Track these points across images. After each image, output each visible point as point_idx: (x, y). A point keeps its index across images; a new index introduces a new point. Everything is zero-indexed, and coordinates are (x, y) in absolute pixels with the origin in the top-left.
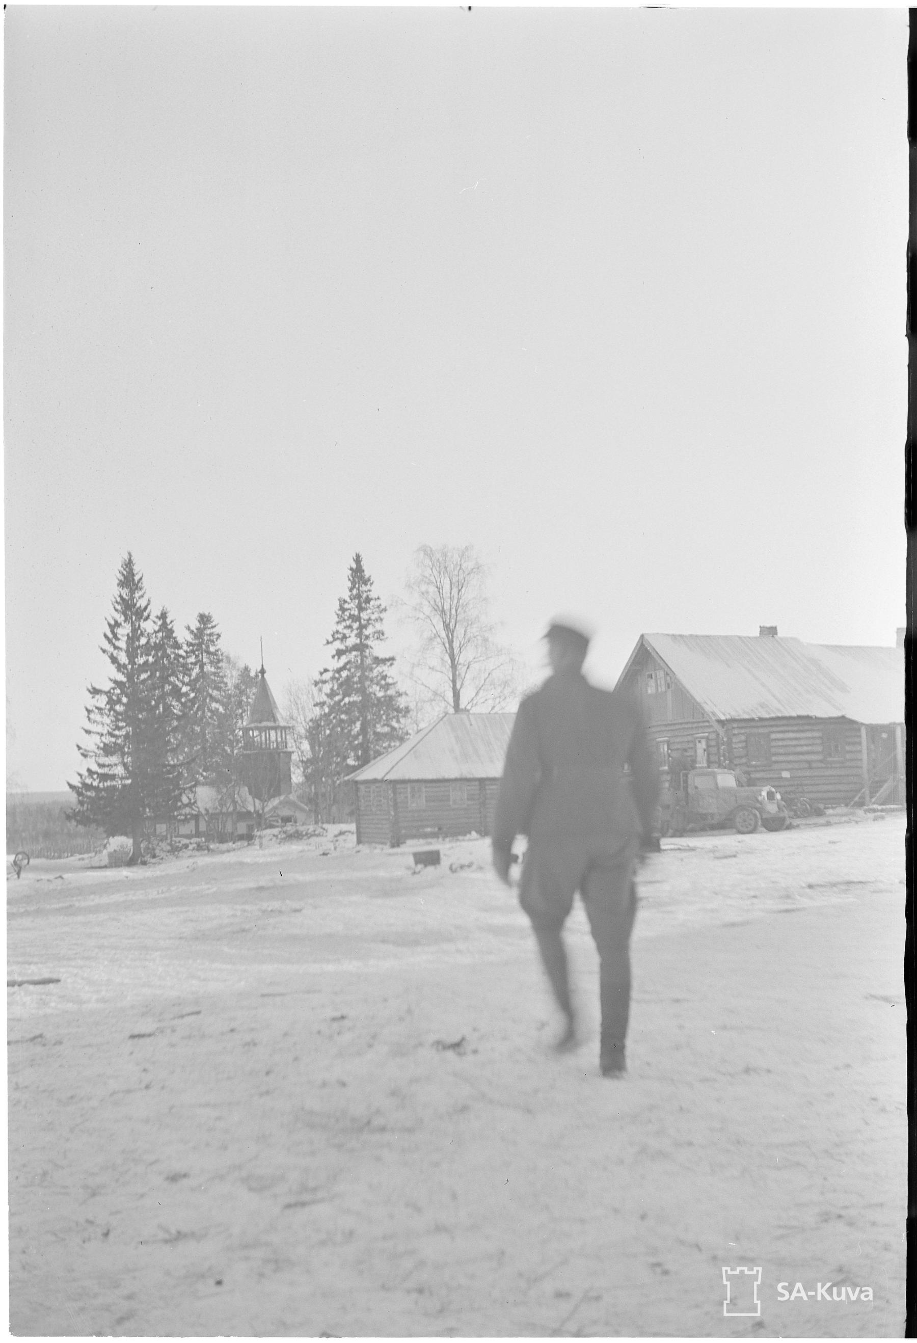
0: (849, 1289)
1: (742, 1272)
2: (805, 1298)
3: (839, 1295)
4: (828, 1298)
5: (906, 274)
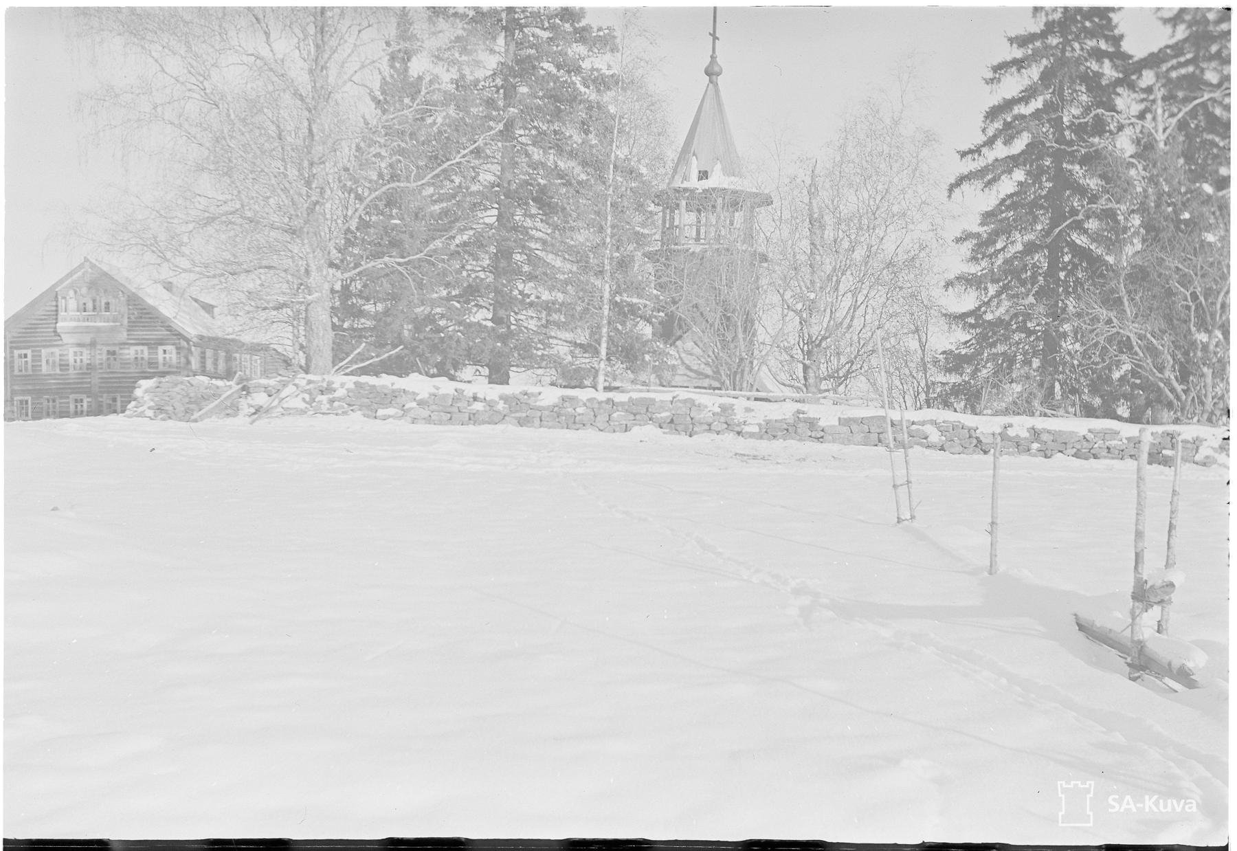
0: (1175, 802)
1: (1067, 783)
2: (1134, 810)
3: (1165, 807)
4: (1155, 809)
5: (980, 842)
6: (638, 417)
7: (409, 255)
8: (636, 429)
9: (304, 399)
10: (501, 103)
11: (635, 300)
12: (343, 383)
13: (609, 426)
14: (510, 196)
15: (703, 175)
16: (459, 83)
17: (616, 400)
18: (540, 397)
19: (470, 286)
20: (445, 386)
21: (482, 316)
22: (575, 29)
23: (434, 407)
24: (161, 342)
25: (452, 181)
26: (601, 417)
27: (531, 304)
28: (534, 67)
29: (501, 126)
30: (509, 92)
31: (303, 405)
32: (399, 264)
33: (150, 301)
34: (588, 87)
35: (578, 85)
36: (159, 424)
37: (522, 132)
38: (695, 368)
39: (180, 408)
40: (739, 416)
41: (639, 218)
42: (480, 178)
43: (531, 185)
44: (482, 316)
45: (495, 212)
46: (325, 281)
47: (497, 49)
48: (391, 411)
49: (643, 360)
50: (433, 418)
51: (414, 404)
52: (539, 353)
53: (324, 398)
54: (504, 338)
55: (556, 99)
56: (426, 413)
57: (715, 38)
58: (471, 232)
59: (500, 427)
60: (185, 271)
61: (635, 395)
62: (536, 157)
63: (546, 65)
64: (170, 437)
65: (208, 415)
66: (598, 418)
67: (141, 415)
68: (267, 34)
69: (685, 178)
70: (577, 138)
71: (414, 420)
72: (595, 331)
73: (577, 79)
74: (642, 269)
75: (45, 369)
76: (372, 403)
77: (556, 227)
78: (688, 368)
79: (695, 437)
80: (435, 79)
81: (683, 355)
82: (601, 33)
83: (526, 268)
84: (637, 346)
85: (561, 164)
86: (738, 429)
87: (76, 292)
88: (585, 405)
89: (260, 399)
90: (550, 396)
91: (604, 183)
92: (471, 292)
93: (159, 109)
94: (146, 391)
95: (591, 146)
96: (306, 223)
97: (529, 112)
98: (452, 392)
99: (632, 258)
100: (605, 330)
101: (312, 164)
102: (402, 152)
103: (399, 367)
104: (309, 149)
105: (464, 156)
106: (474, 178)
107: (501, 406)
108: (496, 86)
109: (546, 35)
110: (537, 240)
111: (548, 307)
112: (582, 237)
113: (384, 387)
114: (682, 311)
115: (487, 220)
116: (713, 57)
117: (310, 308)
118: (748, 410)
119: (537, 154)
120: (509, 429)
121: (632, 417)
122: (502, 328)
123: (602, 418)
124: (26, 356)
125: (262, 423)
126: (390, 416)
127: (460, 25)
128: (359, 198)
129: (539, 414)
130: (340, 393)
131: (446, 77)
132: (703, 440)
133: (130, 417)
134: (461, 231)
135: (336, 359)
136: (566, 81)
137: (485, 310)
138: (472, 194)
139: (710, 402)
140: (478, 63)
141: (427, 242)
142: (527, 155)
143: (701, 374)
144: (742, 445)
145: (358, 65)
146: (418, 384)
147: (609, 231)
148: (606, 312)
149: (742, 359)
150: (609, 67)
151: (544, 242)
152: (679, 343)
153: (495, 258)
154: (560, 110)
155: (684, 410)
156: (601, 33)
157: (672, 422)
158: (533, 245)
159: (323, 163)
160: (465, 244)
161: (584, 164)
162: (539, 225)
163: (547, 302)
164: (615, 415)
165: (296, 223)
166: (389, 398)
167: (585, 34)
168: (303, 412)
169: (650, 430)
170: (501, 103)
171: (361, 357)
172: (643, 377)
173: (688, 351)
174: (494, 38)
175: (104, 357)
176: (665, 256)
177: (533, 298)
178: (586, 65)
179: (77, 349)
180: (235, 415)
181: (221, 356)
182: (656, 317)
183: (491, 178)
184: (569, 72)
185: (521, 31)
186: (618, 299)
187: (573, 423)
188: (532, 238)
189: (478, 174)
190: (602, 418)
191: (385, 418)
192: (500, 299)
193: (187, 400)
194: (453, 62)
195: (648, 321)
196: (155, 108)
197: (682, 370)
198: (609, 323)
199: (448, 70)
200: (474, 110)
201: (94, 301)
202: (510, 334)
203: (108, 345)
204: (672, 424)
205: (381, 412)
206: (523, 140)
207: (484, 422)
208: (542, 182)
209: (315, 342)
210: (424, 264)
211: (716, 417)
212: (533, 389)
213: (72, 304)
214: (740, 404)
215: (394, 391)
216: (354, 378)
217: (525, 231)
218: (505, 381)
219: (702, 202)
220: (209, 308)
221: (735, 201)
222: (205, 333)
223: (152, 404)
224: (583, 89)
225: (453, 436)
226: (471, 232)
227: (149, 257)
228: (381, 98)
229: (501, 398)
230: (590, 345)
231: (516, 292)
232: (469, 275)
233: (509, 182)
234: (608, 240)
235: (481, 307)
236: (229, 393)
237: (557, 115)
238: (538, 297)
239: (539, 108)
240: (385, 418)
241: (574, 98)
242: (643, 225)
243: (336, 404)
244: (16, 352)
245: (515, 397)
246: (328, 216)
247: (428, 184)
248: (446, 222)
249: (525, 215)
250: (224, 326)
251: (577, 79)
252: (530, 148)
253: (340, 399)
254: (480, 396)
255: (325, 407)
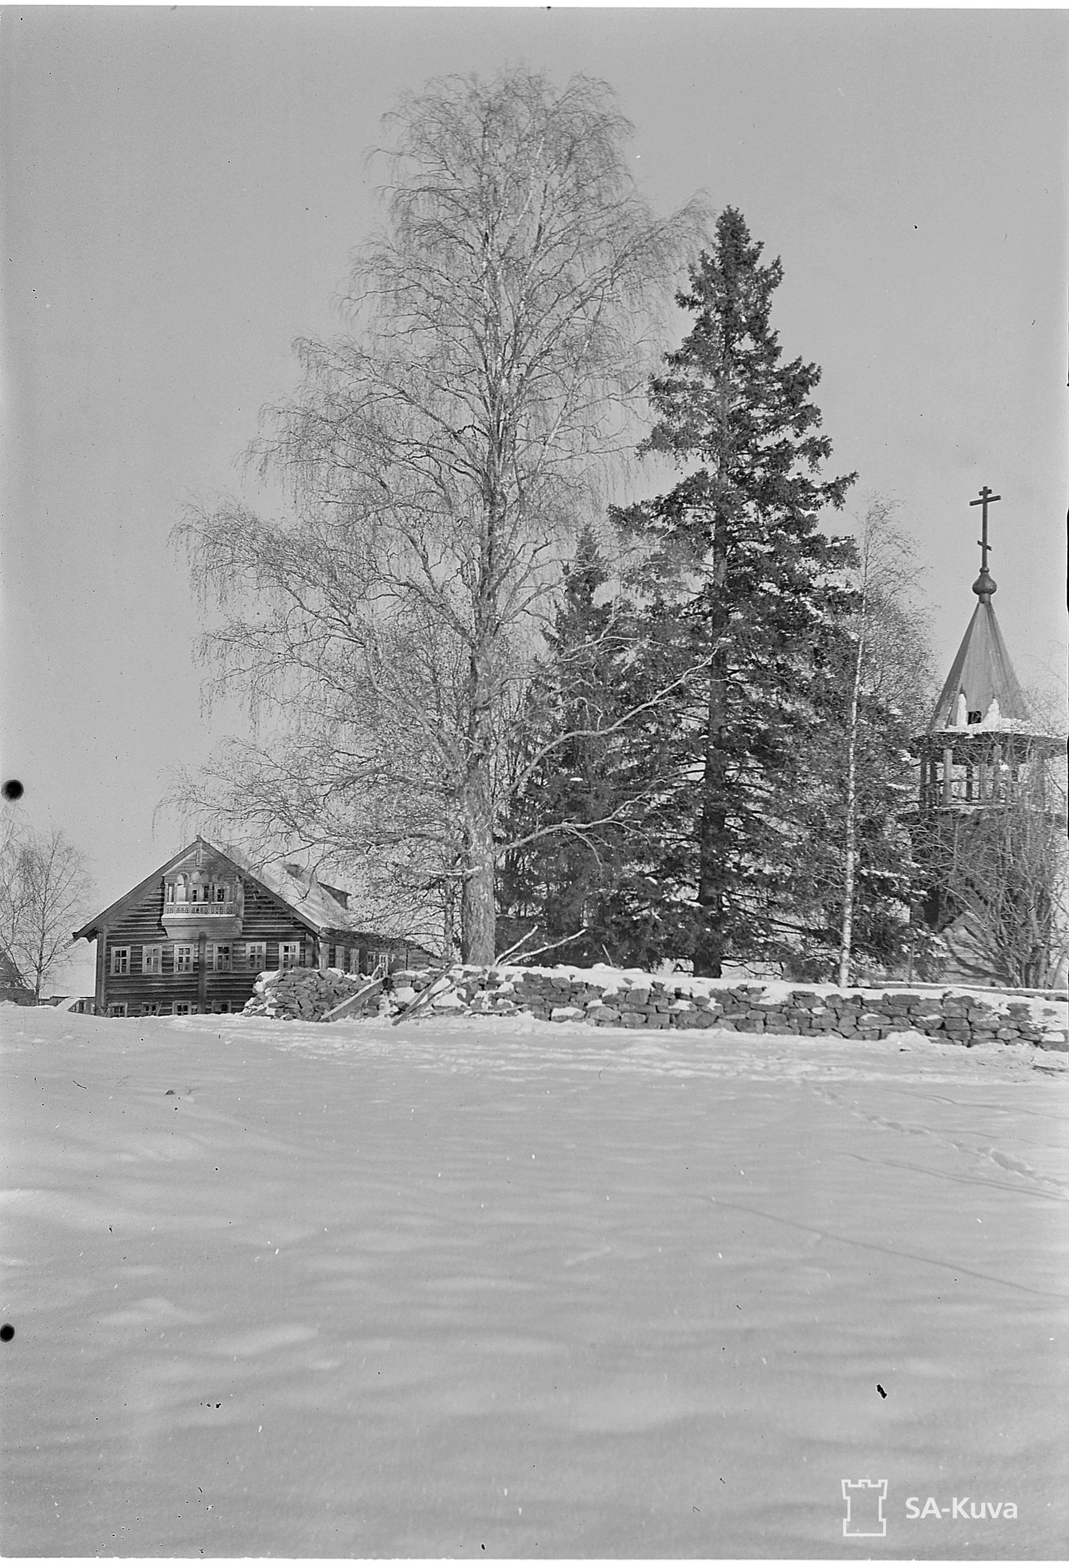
6: (896, 1020)
7: (593, 819)
8: (893, 1036)
9: (459, 995)
10: (709, 633)
11: (887, 874)
12: (510, 974)
13: (857, 1030)
14: (721, 745)
15: (974, 717)
16: (657, 609)
17: (866, 998)
18: (764, 994)
19: (669, 859)
20: (640, 979)
21: (687, 895)
22: (803, 540)
23: (626, 1006)
24: (286, 937)
25: (647, 730)
26: (848, 1018)
27: (751, 880)
28: (751, 588)
29: (709, 660)
30: (720, 619)
31: (459, 1003)
32: (579, 830)
33: (275, 890)
34: (821, 609)
35: (809, 607)
36: (281, 1023)
37: (736, 667)
38: (972, 963)
39: (308, 1006)
40: (1037, 1020)
41: (888, 772)
42: (683, 725)
43: (749, 731)
44: (687, 895)
45: (702, 766)
46: (488, 856)
47: (704, 568)
48: (570, 1011)
49: (900, 951)
50: (624, 1019)
51: (599, 1002)
52: (761, 940)
53: (484, 994)
54: (715, 922)
55: (781, 625)
56: (616, 1014)
57: (986, 548)
58: (672, 792)
59: (711, 1032)
60: (318, 841)
61: (892, 992)
62: (754, 697)
63: (766, 586)
64: (300, 1035)
65: (342, 1014)
66: (843, 1021)
67: (262, 1013)
68: (425, 559)
69: (951, 721)
70: (807, 672)
71: (599, 1023)
72: (835, 913)
73: (807, 601)
74: (897, 835)
75: (145, 969)
76: (546, 999)
77: (781, 784)
78: (961, 962)
79: (976, 1047)
80: (627, 606)
81: (955, 947)
82: (837, 544)
83: (742, 836)
84: (892, 930)
85: (788, 707)
86: (1036, 1037)
87: (185, 877)
88: (824, 1004)
89: (406, 994)
90: (778, 990)
91: (844, 726)
92: (673, 865)
93: (295, 650)
94: (267, 985)
95: (827, 681)
96: (466, 780)
97: (744, 641)
98: (648, 986)
99: (882, 823)
100: (848, 911)
101: (474, 711)
102: (585, 691)
103: (580, 956)
104: (471, 691)
105: (662, 697)
106: (675, 725)
107: (712, 1004)
108: (702, 613)
109: (768, 549)
110: (757, 799)
111: (772, 883)
112: (817, 793)
113: (562, 980)
114: (953, 886)
115: (692, 777)
116: (984, 571)
117: (468, 885)
118: (1048, 1012)
119: (755, 694)
120: (724, 1034)
121: (888, 1021)
122: (712, 912)
123: (847, 1022)
124: (124, 953)
125: (408, 1023)
126: (567, 1018)
127: (658, 541)
128: (529, 756)
129: (763, 1015)
130: (506, 987)
131: (642, 602)
132: (987, 1050)
133: (248, 1015)
134: (660, 788)
135: (499, 948)
136: (793, 603)
137: (688, 889)
138: (673, 743)
139: (997, 1000)
140: (679, 586)
141: (615, 805)
142: (743, 695)
143: (980, 970)
144: (1041, 1056)
145: (533, 591)
146: (605, 976)
147: (852, 785)
148: (850, 888)
149: (1036, 949)
150: (848, 585)
151: (766, 801)
152: (947, 930)
153: (703, 823)
154: (785, 639)
155: (959, 1012)
156: (837, 544)
157: (943, 1026)
158: (750, 806)
159: (487, 708)
160: (664, 807)
161: (817, 702)
162: (759, 781)
163: (772, 876)
164: (865, 1017)
165: (456, 781)
166: (571, 993)
167: (817, 546)
168: (458, 1011)
169: (913, 1038)
170: (709, 633)
171: (529, 946)
172: (898, 973)
173: (963, 937)
174: (700, 556)
175: (216, 955)
176: (931, 814)
177: (752, 871)
178: (818, 583)
179: (185, 946)
180: (375, 1015)
181: (359, 947)
182: (916, 896)
183: (695, 725)
184: (796, 592)
185: (735, 546)
186: (864, 872)
187: (809, 1026)
188: (749, 796)
189: (680, 720)
190: (847, 1022)
191: (562, 1019)
192: (709, 873)
193: (317, 996)
194: (647, 585)
195: (905, 901)
196: (291, 649)
197: (953, 965)
198: (854, 902)
199: (642, 596)
200: (675, 642)
201: (206, 888)
202: (722, 918)
203: (219, 941)
204: (943, 1030)
205: (556, 1012)
206: (738, 676)
207: (690, 1026)
208: (763, 726)
209: (475, 927)
210: (612, 830)
211: (1004, 1022)
212: (754, 983)
213: (181, 891)
214: (1036, 1005)
215: (573, 985)
216: (524, 970)
217: (739, 788)
218: (717, 974)
219: (976, 750)
220: (342, 896)
221: (1018, 747)
222: (337, 926)
223: (274, 1001)
224: (814, 611)
225: (650, 1041)
226: (672, 792)
227: (278, 825)
228: (557, 636)
229: (712, 994)
230: (829, 931)
231: (729, 865)
232: (667, 846)
233: (720, 729)
234: (851, 796)
235: (684, 883)
236: (367, 987)
237: (782, 644)
238: (760, 871)
239: (759, 637)
240: (562, 1019)
241: (805, 620)
242: (896, 779)
243: (500, 1001)
244: (114, 949)
245: (730, 993)
246: (492, 774)
247: (620, 732)
248: (630, 785)
249: (740, 770)
250: (362, 914)
251: (807, 601)
252: (746, 687)
253: (505, 996)
254: (686, 991)
255: (486, 1006)
